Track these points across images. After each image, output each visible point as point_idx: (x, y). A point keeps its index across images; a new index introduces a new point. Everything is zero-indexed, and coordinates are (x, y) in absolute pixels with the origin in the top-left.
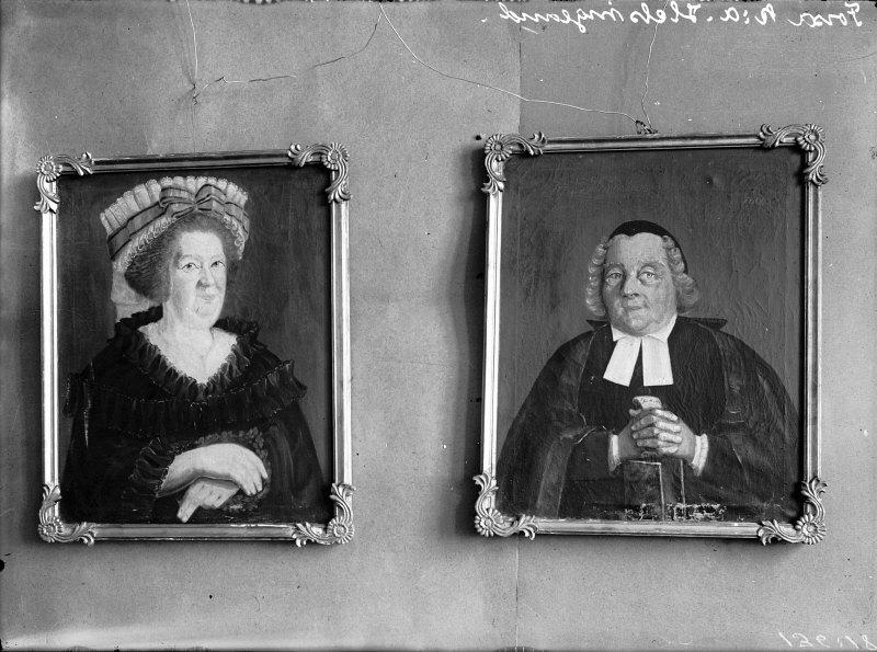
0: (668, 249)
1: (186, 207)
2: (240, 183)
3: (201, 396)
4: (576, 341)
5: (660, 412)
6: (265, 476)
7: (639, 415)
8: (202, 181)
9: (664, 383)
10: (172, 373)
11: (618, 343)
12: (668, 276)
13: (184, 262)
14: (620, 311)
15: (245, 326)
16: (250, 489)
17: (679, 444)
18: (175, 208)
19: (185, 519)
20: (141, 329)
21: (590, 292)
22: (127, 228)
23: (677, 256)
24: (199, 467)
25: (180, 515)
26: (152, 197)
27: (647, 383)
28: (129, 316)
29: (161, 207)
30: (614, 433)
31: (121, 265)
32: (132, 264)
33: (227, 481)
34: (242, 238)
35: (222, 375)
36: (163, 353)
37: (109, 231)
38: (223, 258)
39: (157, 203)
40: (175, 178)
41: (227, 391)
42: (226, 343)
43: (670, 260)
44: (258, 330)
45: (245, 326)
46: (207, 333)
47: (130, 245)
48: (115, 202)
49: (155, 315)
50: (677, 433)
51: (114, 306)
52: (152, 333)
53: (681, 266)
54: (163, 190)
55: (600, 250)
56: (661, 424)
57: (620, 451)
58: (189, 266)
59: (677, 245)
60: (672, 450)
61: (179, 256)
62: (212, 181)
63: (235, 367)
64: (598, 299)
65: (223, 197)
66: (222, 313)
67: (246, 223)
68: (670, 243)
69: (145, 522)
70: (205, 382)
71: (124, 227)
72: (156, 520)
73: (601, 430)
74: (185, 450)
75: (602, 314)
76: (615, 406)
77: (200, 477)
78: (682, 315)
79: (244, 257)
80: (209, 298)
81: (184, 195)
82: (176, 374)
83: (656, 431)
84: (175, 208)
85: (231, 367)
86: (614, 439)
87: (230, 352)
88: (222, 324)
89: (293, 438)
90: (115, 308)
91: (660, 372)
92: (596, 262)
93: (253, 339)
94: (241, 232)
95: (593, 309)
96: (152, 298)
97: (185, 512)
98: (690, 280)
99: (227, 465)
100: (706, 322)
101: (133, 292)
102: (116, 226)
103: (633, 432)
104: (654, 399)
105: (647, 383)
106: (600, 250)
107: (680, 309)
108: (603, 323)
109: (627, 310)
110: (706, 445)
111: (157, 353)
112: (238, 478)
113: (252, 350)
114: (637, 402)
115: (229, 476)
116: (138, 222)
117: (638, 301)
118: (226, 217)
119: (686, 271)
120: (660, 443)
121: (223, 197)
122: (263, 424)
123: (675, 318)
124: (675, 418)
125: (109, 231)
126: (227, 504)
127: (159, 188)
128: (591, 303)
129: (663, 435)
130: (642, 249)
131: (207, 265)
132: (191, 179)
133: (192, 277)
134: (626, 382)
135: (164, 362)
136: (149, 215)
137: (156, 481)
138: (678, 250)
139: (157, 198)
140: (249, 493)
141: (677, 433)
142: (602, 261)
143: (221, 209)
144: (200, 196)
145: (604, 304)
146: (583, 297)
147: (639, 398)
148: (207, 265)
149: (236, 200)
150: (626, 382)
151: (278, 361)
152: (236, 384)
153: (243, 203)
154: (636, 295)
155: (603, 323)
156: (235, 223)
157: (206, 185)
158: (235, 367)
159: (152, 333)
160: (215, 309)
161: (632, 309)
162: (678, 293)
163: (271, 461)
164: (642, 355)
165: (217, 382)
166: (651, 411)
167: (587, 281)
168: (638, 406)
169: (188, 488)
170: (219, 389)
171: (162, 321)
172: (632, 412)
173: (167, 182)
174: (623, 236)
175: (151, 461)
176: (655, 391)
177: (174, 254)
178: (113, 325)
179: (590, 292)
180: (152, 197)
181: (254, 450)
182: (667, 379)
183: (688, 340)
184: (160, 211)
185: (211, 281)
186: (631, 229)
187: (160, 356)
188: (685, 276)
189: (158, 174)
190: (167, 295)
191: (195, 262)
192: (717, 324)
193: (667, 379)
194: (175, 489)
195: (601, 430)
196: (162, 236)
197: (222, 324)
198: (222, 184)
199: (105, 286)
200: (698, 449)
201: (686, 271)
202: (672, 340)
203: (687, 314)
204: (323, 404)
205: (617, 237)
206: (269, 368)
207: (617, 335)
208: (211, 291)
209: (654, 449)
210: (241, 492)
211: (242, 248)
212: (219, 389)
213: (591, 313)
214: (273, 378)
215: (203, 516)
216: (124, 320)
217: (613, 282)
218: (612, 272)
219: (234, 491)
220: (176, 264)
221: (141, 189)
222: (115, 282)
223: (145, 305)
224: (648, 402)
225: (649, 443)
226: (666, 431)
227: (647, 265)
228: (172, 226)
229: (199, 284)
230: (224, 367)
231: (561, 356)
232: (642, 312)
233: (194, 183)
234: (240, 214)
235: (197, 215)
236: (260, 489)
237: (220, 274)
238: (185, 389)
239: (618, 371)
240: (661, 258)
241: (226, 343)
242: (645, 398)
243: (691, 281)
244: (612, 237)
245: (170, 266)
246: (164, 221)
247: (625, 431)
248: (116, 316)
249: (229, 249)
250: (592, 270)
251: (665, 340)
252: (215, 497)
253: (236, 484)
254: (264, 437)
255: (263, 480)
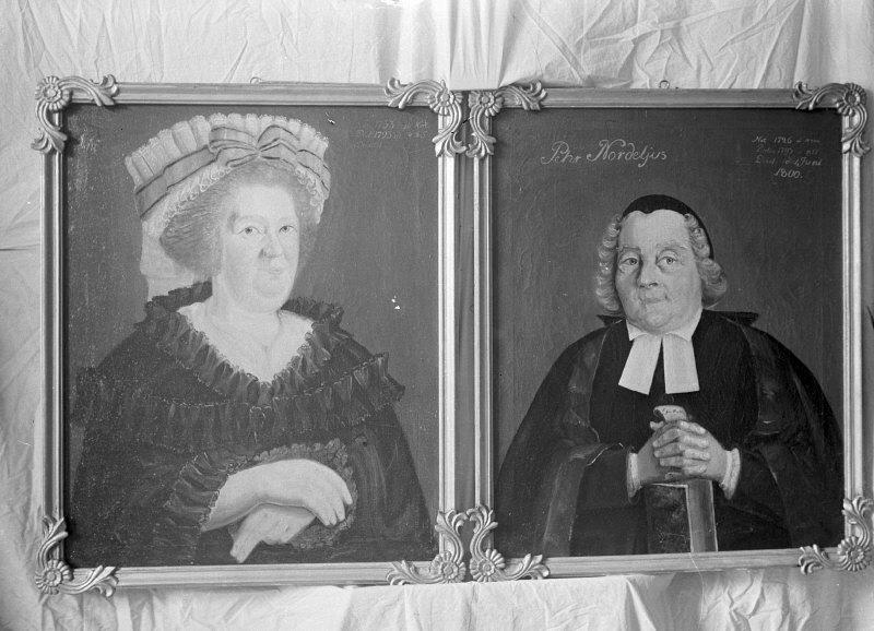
0: (691, 230)
1: (245, 153)
2: (324, 129)
3: (264, 397)
4: (581, 343)
5: (684, 424)
6: (349, 501)
7: (661, 428)
8: (267, 120)
9: (642, 392)
10: (224, 369)
11: (635, 344)
12: (691, 262)
13: (241, 226)
14: (637, 304)
15: (324, 309)
16: (329, 519)
17: (707, 461)
18: (230, 154)
19: (241, 558)
20: (182, 310)
21: (600, 281)
22: (164, 179)
23: (702, 238)
24: (261, 490)
25: (234, 552)
26: (198, 139)
27: (669, 390)
28: (166, 294)
29: (210, 152)
30: (633, 451)
31: (154, 226)
32: (171, 225)
33: (297, 507)
34: (320, 196)
35: (292, 372)
36: (211, 342)
37: (138, 181)
38: (293, 221)
39: (206, 147)
40: (212, 117)
41: (300, 392)
42: (300, 329)
43: (693, 240)
44: (341, 315)
45: (324, 309)
46: (274, 317)
47: (167, 200)
48: (146, 143)
49: (203, 292)
50: (705, 449)
51: (143, 279)
52: (195, 315)
53: (706, 250)
54: (215, 129)
55: (612, 229)
56: (687, 438)
57: (642, 471)
58: (248, 230)
59: (701, 224)
60: (700, 469)
61: (234, 217)
62: (281, 121)
63: (310, 361)
64: (609, 290)
65: (295, 142)
66: (294, 291)
67: (327, 177)
68: (694, 223)
69: (186, 563)
70: (270, 380)
71: (157, 177)
72: (203, 559)
73: (618, 448)
74: (241, 468)
75: (615, 308)
76: (634, 418)
77: (265, 502)
78: (708, 308)
79: (322, 220)
80: (276, 272)
81: (242, 137)
82: (231, 370)
83: (681, 447)
84: (230, 154)
85: (304, 361)
86: (633, 458)
87: (303, 342)
88: (293, 306)
89: (385, 453)
90: (146, 284)
91: (683, 377)
92: (607, 244)
93: (335, 326)
94: (319, 188)
95: (605, 302)
96: (197, 268)
97: (242, 546)
98: (716, 267)
99: (307, 485)
100: (732, 316)
101: (170, 262)
102: (148, 174)
103: (654, 449)
104: (678, 409)
105: (669, 390)
106: (612, 229)
107: (706, 300)
108: (617, 319)
109: (645, 302)
110: (738, 462)
111: (204, 341)
112: (311, 503)
113: (333, 340)
114: (658, 412)
115: (300, 501)
116: (179, 170)
117: (656, 292)
118: (303, 171)
119: (711, 257)
120: (685, 461)
121: (295, 142)
122: (344, 433)
123: (700, 311)
124: (702, 430)
125: (138, 181)
126: (298, 537)
127: (208, 127)
128: (601, 294)
129: (689, 452)
130: (659, 230)
131: (273, 230)
132: (251, 119)
133: (253, 244)
134: (645, 389)
135: (214, 354)
136: (195, 162)
137: (200, 510)
138: (702, 230)
139: (206, 141)
140: (327, 523)
141: (705, 449)
142: (614, 243)
143: (292, 159)
144: (265, 143)
145: (617, 296)
146: (591, 287)
147: (660, 409)
148: (273, 230)
149: (312, 149)
150: (645, 389)
151: (368, 355)
152: (312, 383)
153: (321, 153)
154: (656, 284)
155: (617, 319)
156: (311, 176)
157: (273, 126)
158: (310, 361)
159: (195, 315)
160: (284, 287)
161: (650, 301)
162: (703, 282)
163: (356, 481)
164: (660, 355)
165: (285, 381)
166: (674, 423)
167: (596, 268)
168: (660, 418)
169: (245, 518)
170: (288, 389)
171: (211, 299)
172: (653, 425)
173: (219, 119)
174: (639, 213)
175: (194, 483)
176: (679, 399)
177: (228, 215)
178: (142, 307)
179: (600, 281)
180: (198, 139)
181: (334, 468)
182: (692, 385)
183: (718, 336)
184: (210, 158)
185: (279, 250)
186: (649, 204)
187: (207, 347)
188: (711, 262)
189: (208, 109)
190: (218, 266)
191: (257, 225)
192: (747, 318)
193: (692, 385)
194: (231, 517)
195: (618, 448)
196: (211, 191)
197: (293, 306)
198: (294, 125)
199: (133, 255)
200: (728, 466)
201: (711, 257)
202: (695, 338)
203: (711, 308)
204: (72, 457)
205: (632, 214)
206: (355, 363)
207: (633, 334)
208: (277, 263)
209: (678, 469)
210: (317, 522)
211: (320, 209)
212: (288, 389)
213: (602, 307)
214: (361, 376)
215: (266, 553)
216: (159, 300)
217: (627, 270)
218: (625, 257)
219: (308, 520)
220: (231, 227)
221: (182, 128)
222: (145, 250)
223: (187, 280)
224: (670, 412)
225: (673, 462)
226: (695, 446)
227: (667, 249)
228: (225, 178)
229: (262, 253)
230: (295, 361)
231: (568, 360)
232: (662, 306)
233: (254, 123)
234: (318, 165)
235: (259, 163)
236: (342, 517)
237: (291, 242)
238: (242, 388)
239: (635, 376)
240: (683, 240)
241: (300, 329)
242: (668, 408)
243: (718, 268)
244: (625, 214)
245: (223, 229)
246: (214, 172)
247: (645, 449)
248: (146, 295)
249: (302, 209)
250: (602, 254)
251: (689, 338)
252: (284, 528)
253: (309, 511)
254: (349, 451)
255: (346, 507)
